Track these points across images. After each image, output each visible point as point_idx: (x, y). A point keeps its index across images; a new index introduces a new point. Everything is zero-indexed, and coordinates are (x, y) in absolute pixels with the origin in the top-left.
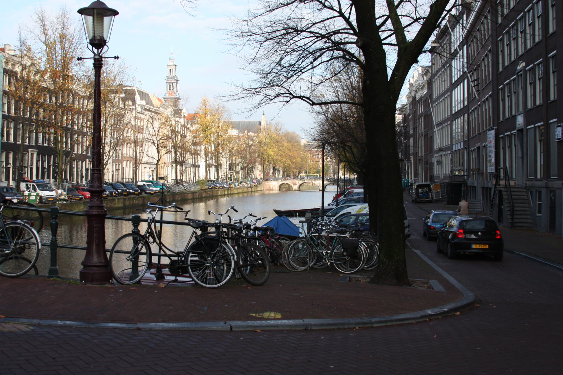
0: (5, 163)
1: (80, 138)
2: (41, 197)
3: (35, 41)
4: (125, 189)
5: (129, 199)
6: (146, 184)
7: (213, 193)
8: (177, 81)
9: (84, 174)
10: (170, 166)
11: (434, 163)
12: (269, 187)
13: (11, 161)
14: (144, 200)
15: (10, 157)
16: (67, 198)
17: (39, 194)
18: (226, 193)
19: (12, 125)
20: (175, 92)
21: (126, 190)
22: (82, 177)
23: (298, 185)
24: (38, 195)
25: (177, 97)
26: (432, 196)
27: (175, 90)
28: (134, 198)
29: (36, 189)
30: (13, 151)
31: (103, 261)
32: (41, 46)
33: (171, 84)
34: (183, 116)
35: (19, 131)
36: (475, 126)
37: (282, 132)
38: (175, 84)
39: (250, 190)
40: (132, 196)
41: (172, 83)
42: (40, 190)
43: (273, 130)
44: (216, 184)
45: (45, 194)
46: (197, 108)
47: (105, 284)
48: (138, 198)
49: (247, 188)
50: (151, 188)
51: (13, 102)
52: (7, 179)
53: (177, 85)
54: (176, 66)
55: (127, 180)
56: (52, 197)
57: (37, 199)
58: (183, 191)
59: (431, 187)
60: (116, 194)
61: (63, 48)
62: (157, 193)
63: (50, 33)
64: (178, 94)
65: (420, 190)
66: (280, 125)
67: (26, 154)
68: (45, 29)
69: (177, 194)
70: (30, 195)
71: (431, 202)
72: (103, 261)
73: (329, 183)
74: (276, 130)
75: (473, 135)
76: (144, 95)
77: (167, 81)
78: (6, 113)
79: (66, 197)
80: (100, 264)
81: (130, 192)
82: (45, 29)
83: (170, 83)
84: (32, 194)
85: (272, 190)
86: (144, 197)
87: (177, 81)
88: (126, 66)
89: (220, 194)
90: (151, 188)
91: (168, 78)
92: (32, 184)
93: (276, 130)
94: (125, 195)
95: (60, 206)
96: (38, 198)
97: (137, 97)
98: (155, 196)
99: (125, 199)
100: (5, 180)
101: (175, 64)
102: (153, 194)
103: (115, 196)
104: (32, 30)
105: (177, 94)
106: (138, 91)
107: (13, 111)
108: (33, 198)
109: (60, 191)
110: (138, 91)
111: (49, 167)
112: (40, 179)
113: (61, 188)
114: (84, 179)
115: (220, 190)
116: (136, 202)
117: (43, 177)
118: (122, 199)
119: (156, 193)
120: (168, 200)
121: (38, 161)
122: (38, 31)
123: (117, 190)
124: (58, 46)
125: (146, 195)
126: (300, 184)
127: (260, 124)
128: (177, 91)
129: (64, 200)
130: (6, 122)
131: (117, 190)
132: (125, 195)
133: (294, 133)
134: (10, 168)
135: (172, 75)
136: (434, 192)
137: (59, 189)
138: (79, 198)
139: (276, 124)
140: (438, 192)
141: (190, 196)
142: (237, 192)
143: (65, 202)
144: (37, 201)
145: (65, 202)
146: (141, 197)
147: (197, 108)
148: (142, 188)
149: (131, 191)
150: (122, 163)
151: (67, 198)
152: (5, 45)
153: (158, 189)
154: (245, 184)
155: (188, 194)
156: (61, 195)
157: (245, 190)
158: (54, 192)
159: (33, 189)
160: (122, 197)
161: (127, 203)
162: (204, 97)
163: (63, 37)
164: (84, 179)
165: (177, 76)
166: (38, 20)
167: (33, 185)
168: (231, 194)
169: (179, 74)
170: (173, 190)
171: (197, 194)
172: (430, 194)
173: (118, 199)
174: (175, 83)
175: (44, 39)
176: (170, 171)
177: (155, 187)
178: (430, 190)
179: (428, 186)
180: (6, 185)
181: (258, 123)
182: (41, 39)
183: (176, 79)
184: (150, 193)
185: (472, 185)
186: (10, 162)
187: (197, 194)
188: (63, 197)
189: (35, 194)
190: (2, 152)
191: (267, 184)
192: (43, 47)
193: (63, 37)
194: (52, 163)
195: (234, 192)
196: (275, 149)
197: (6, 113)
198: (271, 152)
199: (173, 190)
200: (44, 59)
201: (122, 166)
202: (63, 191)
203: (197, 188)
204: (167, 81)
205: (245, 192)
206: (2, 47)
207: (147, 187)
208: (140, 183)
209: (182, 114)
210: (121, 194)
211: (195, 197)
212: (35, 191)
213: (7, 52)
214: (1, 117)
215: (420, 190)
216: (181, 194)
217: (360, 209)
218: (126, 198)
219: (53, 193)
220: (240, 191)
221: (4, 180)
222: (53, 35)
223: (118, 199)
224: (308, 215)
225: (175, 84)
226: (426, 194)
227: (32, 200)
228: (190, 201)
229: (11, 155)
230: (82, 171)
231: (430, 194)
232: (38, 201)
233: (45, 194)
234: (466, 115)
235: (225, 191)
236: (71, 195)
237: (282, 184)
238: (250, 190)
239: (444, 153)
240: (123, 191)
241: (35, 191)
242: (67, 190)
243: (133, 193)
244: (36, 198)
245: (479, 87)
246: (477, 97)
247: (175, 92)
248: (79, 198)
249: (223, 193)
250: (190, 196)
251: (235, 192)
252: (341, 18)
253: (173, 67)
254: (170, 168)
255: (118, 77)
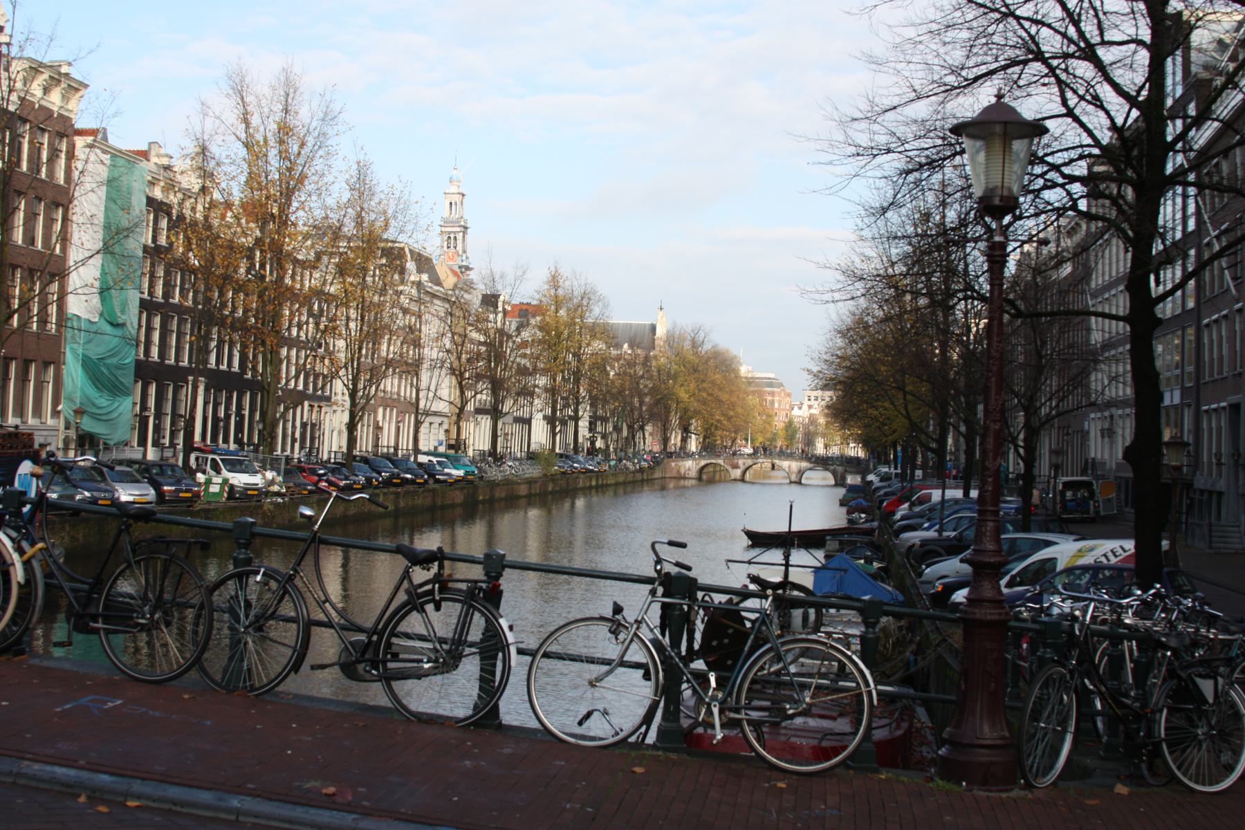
0: (138, 406)
1: (294, 352)
2: (232, 487)
3: (222, 138)
4: (396, 470)
5: (407, 493)
6: (434, 460)
7: (568, 483)
8: (466, 228)
9: (297, 435)
10: (471, 419)
11: (1088, 432)
12: (679, 472)
13: (152, 402)
14: (434, 497)
15: (150, 393)
16: (284, 490)
17: (228, 480)
18: (594, 483)
19: (157, 321)
20: (460, 252)
21: (399, 475)
22: (294, 440)
23: (743, 468)
24: (226, 481)
25: (464, 264)
26: (1095, 507)
27: (459, 248)
28: (414, 493)
29: (221, 469)
30: (156, 380)
31: (1007, 734)
32: (235, 150)
33: (452, 236)
34: (500, 309)
35: (171, 335)
36: (1221, 357)
37: (707, 347)
38: (460, 236)
39: (639, 476)
40: (411, 488)
41: (455, 233)
42: (229, 471)
43: (687, 345)
44: (574, 462)
45: (240, 479)
46: (538, 292)
47: (1012, 790)
48: (423, 492)
49: (633, 472)
50: (446, 470)
51: (160, 273)
52: (143, 442)
53: (464, 237)
54: (463, 195)
55: (385, 450)
56: (253, 487)
57: (224, 490)
58: (510, 477)
59: (1095, 487)
60: (380, 483)
61: (284, 155)
62: (459, 481)
63: (255, 121)
64: (467, 258)
65: (1069, 494)
66: (702, 335)
67: (182, 386)
68: (246, 113)
69: (498, 485)
70: (208, 482)
71: (1093, 521)
72: (1007, 734)
73: (812, 465)
74: (693, 342)
75: (1211, 375)
76: (424, 263)
77: (443, 229)
78: (146, 296)
79: (281, 487)
80: (999, 742)
81: (407, 479)
82: (246, 113)
83: (450, 233)
84: (215, 480)
85: (685, 478)
86: (434, 490)
87: (466, 228)
88: (413, 199)
89: (581, 485)
90: (446, 470)
91: (446, 222)
92: (211, 457)
93: (693, 342)
94: (396, 485)
95: (271, 507)
96: (227, 489)
97: (411, 265)
98: (457, 489)
99: (397, 494)
100: (138, 446)
101: (461, 190)
102: (451, 484)
103: (377, 487)
104: (218, 114)
105: (464, 258)
106: (411, 251)
107: (159, 291)
108: (214, 489)
109: (270, 475)
110: (411, 251)
111: (228, 416)
112: (209, 443)
113: (268, 467)
114: (297, 445)
115: (582, 476)
116: (419, 501)
117: (214, 438)
118: (391, 493)
119: (459, 481)
120: (481, 498)
121: (206, 403)
122: (232, 116)
123: (379, 473)
124: (273, 153)
125: (436, 486)
126: (747, 465)
127: (653, 328)
128: (464, 252)
129: (278, 494)
130: (144, 316)
131: (379, 473)
132: (396, 485)
133: (727, 351)
134: (148, 417)
135: (455, 216)
136: (1100, 499)
137: (266, 470)
138: (306, 490)
139: (693, 331)
140: (1109, 500)
141: (523, 490)
142: (613, 482)
143: (280, 500)
144: (223, 496)
145: (280, 500)
146: (429, 491)
147: (538, 292)
148: (427, 468)
149: (409, 476)
150: (376, 412)
151: (284, 490)
152: (150, 144)
153: (461, 473)
154: (629, 464)
155: (519, 484)
156: (272, 482)
157: (630, 478)
158: (259, 476)
159: (212, 468)
160: (392, 489)
161: (402, 504)
162: (553, 269)
163: (285, 131)
164: (297, 445)
165: (465, 217)
166: (231, 92)
167: (213, 460)
168: (602, 486)
169: (470, 213)
170: (489, 474)
171: (538, 485)
172: (1092, 502)
173: (385, 494)
174: (461, 234)
175: (243, 136)
176: (472, 431)
177: (455, 468)
178: (1092, 494)
179: (1088, 485)
180: (139, 456)
181: (647, 330)
182: (238, 133)
183: (462, 223)
184: (445, 481)
185: (1209, 488)
186: (149, 406)
187: (538, 485)
188: (276, 488)
189: (220, 480)
190: (136, 382)
191: (673, 464)
192: (239, 152)
193: (285, 131)
194: (234, 409)
195: (609, 482)
196: (693, 385)
197: (146, 296)
198: (683, 395)
199: (489, 474)
200: (243, 179)
201: (375, 417)
202: (275, 474)
203: (533, 471)
204: (443, 229)
205: (630, 483)
206: (145, 148)
207: (438, 467)
208: (423, 459)
209: (500, 304)
210: (388, 483)
211: (533, 492)
212: (218, 472)
213: (154, 159)
214: (138, 304)
215: (1069, 494)
216: (507, 484)
217: (1080, 551)
218: (399, 493)
219: (257, 480)
220: (621, 479)
221: (136, 446)
222: (265, 127)
223: (385, 494)
224: (832, 545)
225: (460, 236)
226: (1082, 504)
227: (214, 494)
228: (523, 502)
229: (152, 390)
230: (294, 426)
231: (1092, 502)
232: (225, 495)
233: (240, 479)
234: (1191, 331)
235: (591, 480)
236: (291, 484)
237: (706, 465)
238: (639, 476)
239: (1120, 412)
240: (393, 476)
241: (218, 472)
242: (282, 473)
243: (412, 482)
244: (222, 489)
245: (1236, 270)
246: (1234, 291)
247: (460, 252)
248: (306, 490)
249: (588, 484)
250: (523, 490)
251: (611, 481)
252: (1069, 120)
253: (457, 198)
254: (472, 425)
255: (392, 222)
